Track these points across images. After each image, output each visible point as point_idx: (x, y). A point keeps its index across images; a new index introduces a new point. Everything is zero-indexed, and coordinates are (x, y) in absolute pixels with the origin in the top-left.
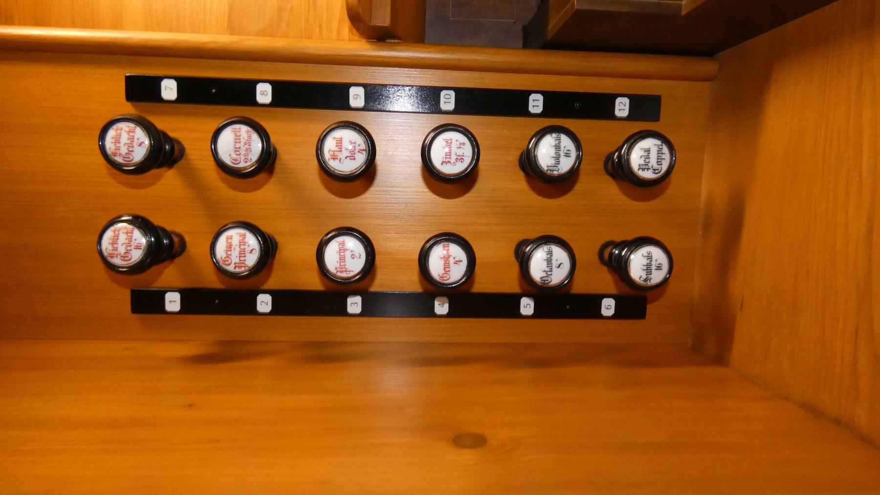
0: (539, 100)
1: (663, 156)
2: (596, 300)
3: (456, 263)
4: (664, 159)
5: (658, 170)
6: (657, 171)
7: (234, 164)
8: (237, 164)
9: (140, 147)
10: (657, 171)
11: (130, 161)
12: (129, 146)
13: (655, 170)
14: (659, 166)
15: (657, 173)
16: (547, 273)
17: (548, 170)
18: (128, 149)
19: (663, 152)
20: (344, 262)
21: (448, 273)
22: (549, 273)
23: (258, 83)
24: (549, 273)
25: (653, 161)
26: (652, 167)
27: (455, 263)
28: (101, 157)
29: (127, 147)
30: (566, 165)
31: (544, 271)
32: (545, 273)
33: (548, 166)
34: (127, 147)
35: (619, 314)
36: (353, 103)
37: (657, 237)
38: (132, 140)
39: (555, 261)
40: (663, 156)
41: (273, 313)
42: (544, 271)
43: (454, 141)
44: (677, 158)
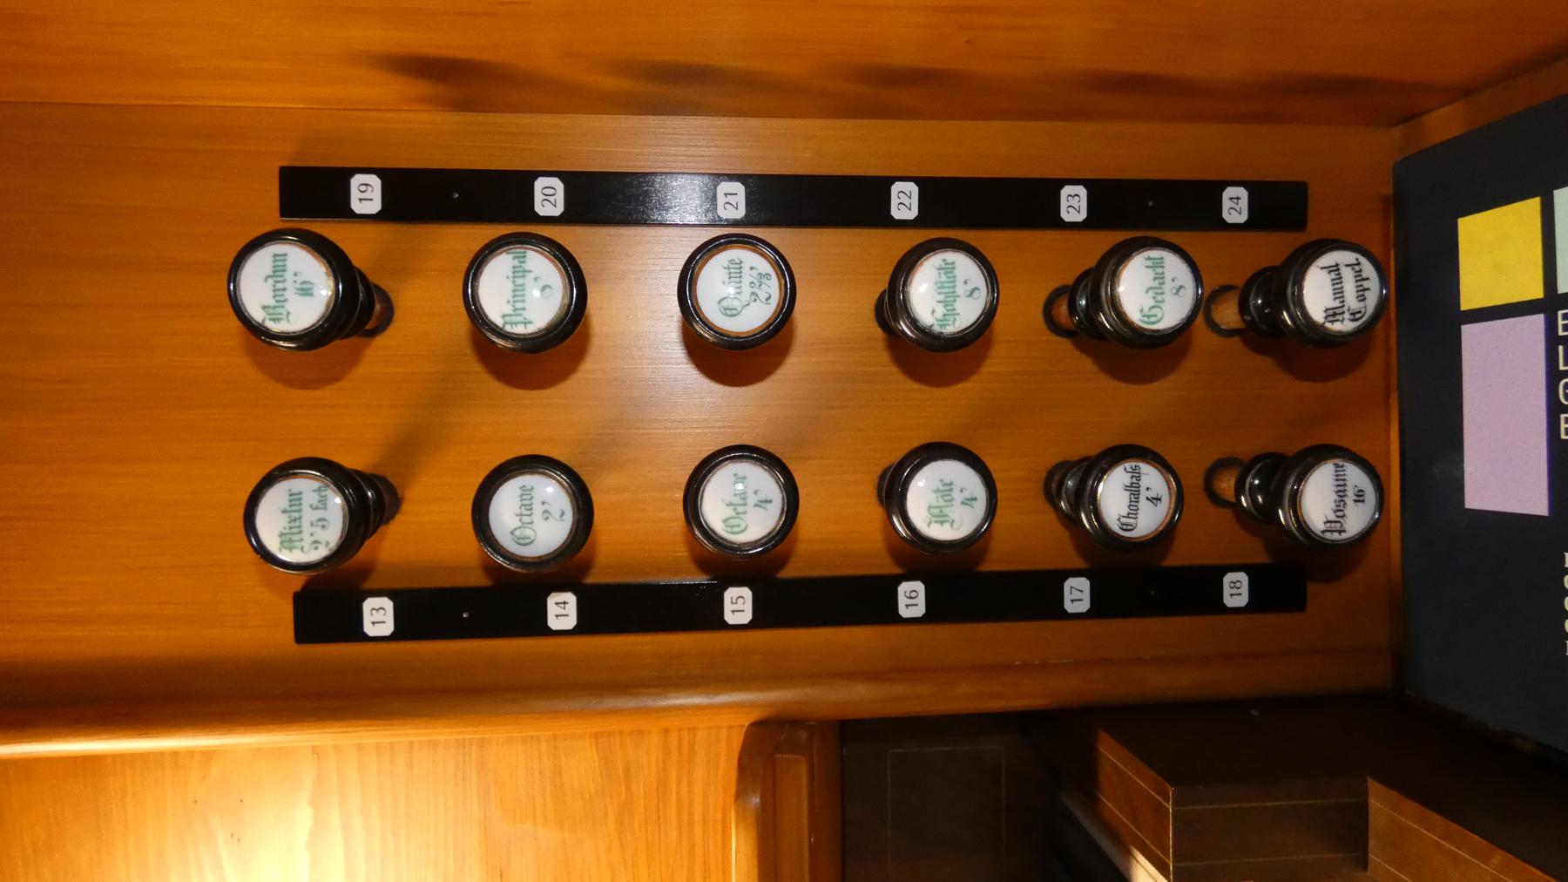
0: (736, 194)
1: (1366, 285)
2: (1212, 578)
3: (967, 504)
4: (1368, 289)
5: (1360, 312)
6: (1358, 316)
7: (1146, 323)
8: (1153, 323)
9: (1177, 296)
10: (1358, 316)
11: (1153, 323)
12: (1156, 293)
13: (1354, 314)
14: (1362, 304)
15: (1358, 319)
16: (735, 510)
17: (506, 323)
18: (1154, 298)
19: (1365, 275)
20: (1135, 518)
21: (741, 516)
22: (740, 509)
23: (352, 176)
24: (740, 509)
25: (1351, 301)
26: (1349, 310)
27: (963, 503)
28: (235, 318)
29: (1153, 295)
30: (967, 313)
31: (730, 504)
32: (731, 508)
33: (504, 316)
34: (1153, 295)
35: (1257, 603)
36: (543, 208)
37: (1148, 445)
38: (1161, 281)
39: (959, 492)
40: (1366, 285)
41: (927, 619)
42: (730, 504)
43: (746, 270)
44: (1001, 295)
